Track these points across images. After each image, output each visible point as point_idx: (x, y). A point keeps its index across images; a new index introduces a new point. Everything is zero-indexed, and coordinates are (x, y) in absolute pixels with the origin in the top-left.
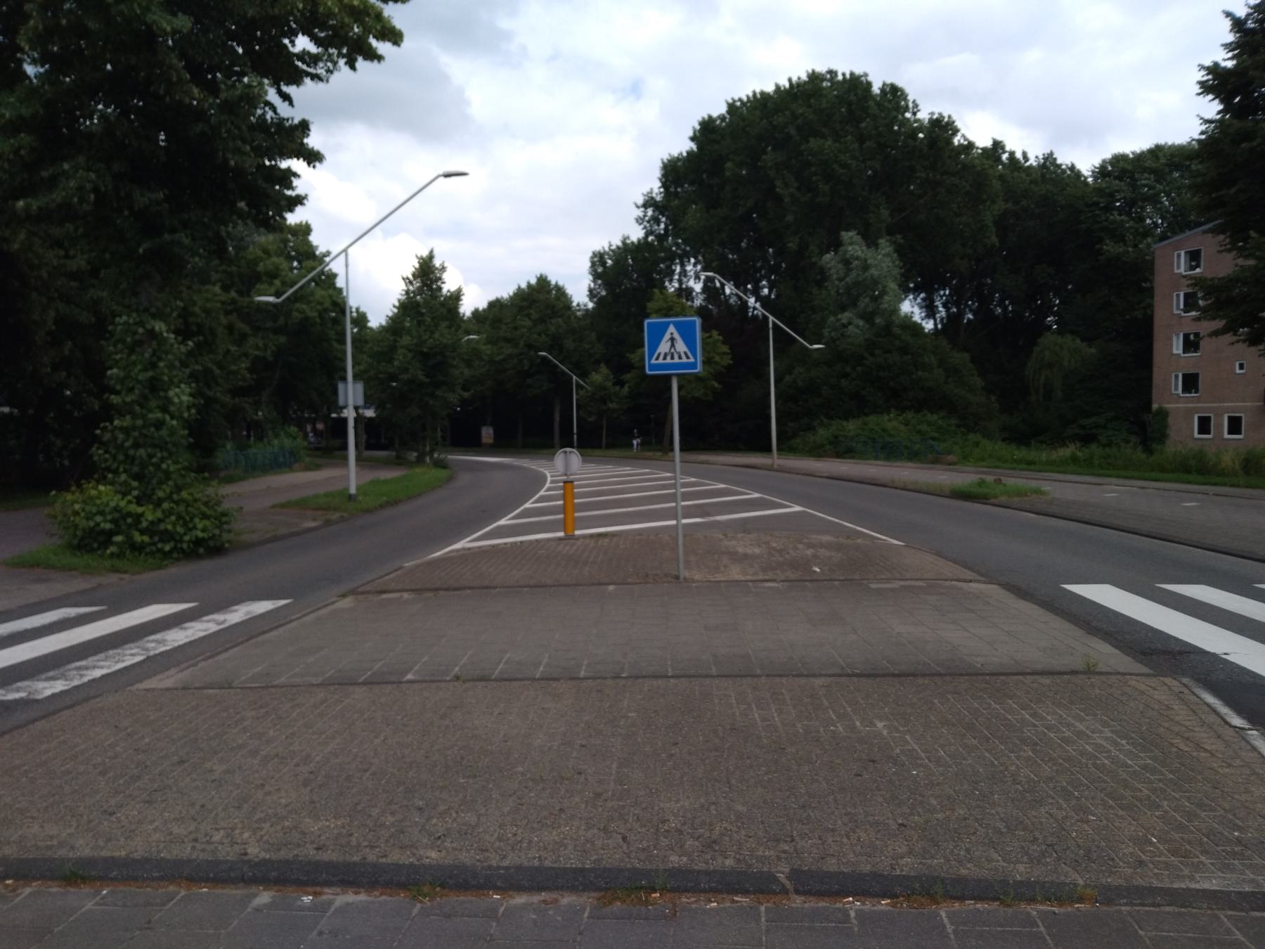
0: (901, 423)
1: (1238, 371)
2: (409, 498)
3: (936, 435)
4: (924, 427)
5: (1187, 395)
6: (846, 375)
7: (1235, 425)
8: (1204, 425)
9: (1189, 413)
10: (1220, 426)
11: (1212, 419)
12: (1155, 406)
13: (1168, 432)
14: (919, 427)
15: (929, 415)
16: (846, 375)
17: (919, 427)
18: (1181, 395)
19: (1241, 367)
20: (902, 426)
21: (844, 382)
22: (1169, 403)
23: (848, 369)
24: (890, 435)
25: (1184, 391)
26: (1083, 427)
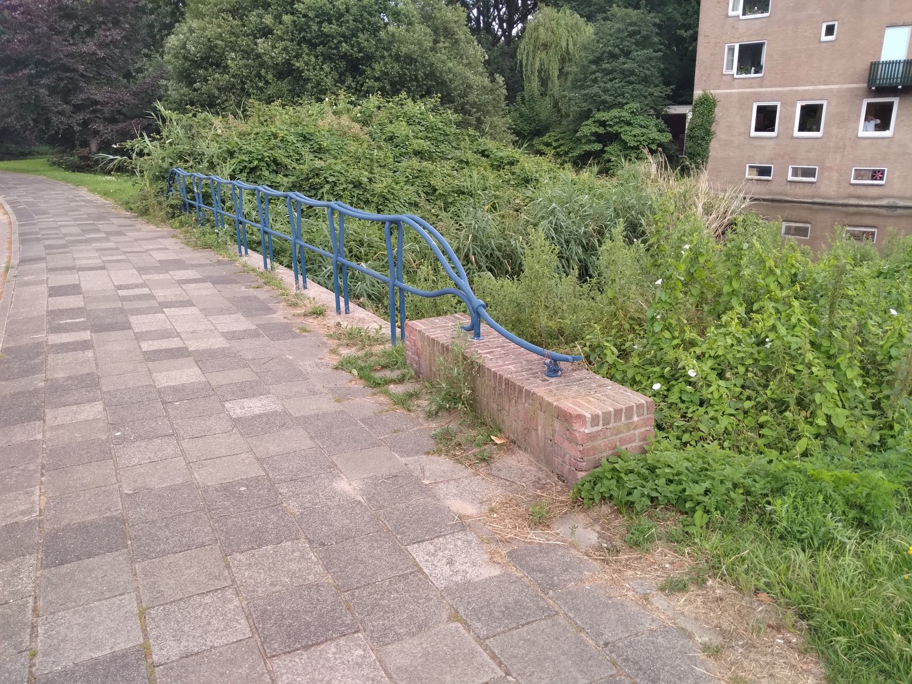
0: (355, 119)
1: (824, 38)
2: (752, 180)
3: (425, 145)
4: (401, 129)
5: (744, 76)
6: (266, 32)
7: (766, 118)
8: (766, 118)
9: (743, 101)
10: (789, 119)
11: (804, 103)
12: (698, 93)
13: (713, 128)
14: (390, 128)
15: (410, 102)
16: (266, 32)
17: (390, 128)
18: (736, 76)
19: (830, 30)
20: (357, 126)
21: (262, 45)
22: (718, 88)
23: (268, 20)
24: (319, 151)
25: (740, 69)
26: (603, 124)
